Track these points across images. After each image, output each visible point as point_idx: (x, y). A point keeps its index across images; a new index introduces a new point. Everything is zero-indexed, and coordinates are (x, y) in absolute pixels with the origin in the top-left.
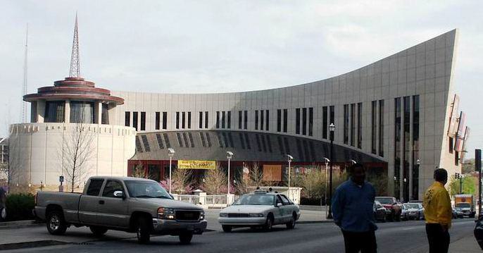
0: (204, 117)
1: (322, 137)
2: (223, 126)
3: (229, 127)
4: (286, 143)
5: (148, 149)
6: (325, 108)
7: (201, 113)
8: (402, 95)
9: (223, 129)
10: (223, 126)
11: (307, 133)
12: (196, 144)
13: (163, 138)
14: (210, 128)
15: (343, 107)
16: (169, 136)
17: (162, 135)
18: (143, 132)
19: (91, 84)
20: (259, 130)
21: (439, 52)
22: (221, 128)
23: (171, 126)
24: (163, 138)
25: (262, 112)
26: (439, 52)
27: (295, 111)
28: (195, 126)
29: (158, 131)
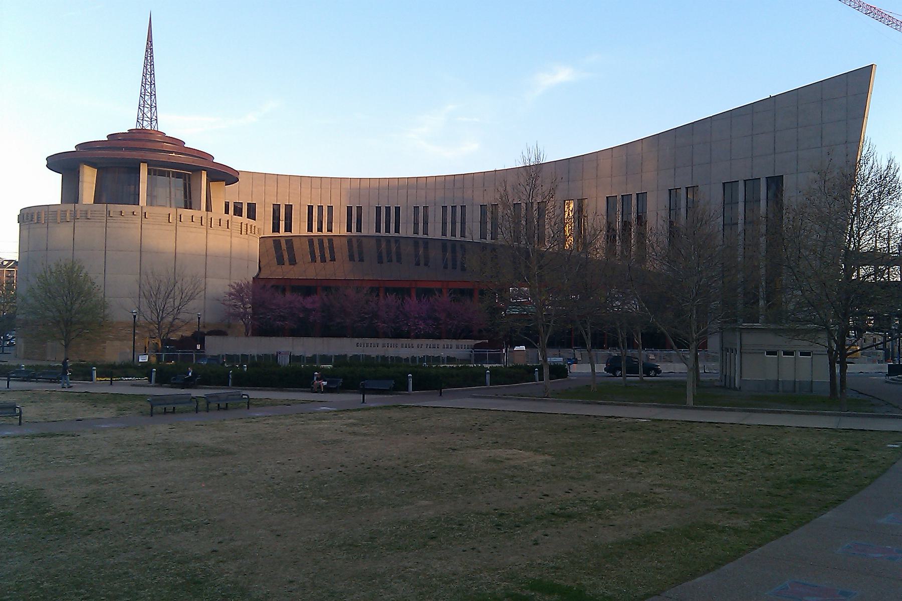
0: (354, 216)
1: (314, 239)
2: (388, 230)
3: (397, 230)
4: (454, 251)
5: (293, 262)
6: (276, 209)
7: (310, 208)
8: (741, 173)
9: (320, 234)
10: (388, 230)
11: (489, 237)
12: (338, 255)
13: (284, 246)
14: (295, 231)
15: (668, 192)
16: (336, 242)
17: (283, 242)
18: (288, 234)
19: (179, 143)
20: (449, 236)
21: (867, 71)
22: (282, 232)
23: (299, 228)
24: (284, 246)
25: (388, 209)
26: (867, 71)
27: (411, 211)
28: (339, 229)
29: (378, 234)
